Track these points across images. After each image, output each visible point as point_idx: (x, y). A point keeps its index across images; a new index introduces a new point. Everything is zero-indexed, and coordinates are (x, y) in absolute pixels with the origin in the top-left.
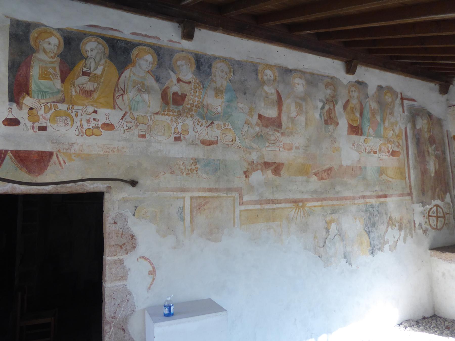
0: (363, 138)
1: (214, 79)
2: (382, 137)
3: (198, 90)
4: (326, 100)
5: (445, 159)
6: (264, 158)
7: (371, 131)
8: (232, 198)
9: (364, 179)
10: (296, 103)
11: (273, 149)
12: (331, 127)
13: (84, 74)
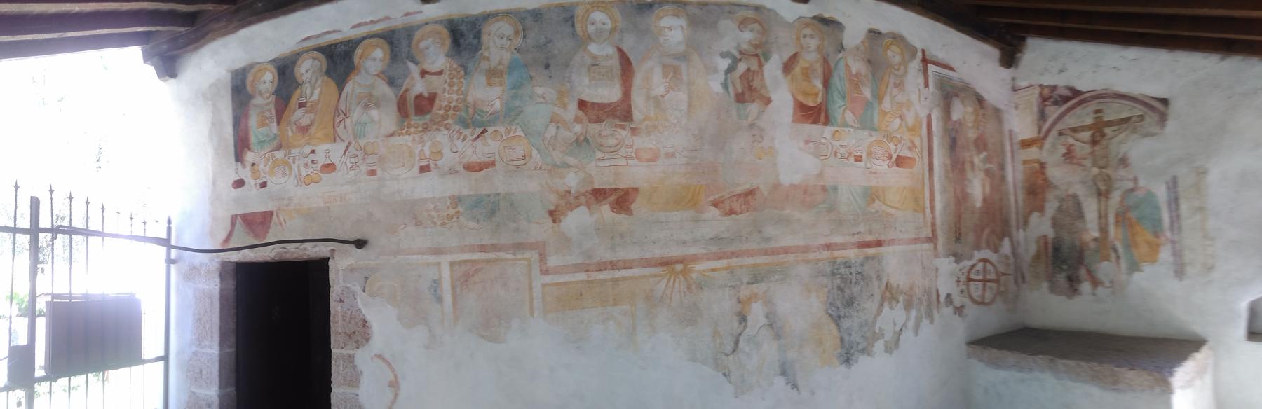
0: (828, 131)
1: (486, 54)
2: (876, 130)
3: (455, 80)
4: (741, 53)
5: (1003, 179)
6: (592, 183)
7: (849, 117)
8: (525, 262)
9: (832, 209)
10: (664, 66)
11: (613, 162)
12: (753, 108)
13: (301, 105)
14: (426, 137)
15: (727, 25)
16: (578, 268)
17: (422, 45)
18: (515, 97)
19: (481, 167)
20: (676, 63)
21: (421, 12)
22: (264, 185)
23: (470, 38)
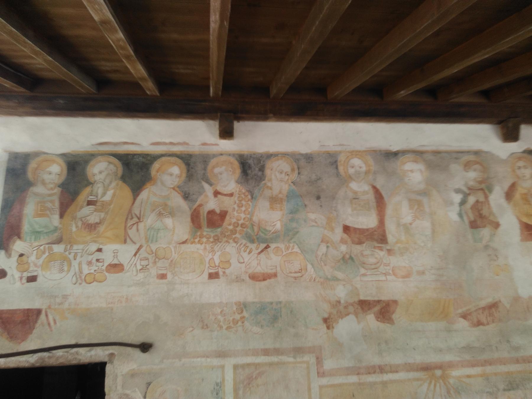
1: (269, 184)
3: (244, 202)
4: (469, 189)
6: (358, 295)
8: (304, 365)
10: (410, 200)
12: (486, 232)
13: (90, 203)
14: (216, 248)
15: (455, 167)
16: (349, 371)
17: (217, 170)
18: (292, 220)
19: (265, 277)
20: (419, 198)
21: (217, 145)
22: (32, 279)
23: (256, 171)
